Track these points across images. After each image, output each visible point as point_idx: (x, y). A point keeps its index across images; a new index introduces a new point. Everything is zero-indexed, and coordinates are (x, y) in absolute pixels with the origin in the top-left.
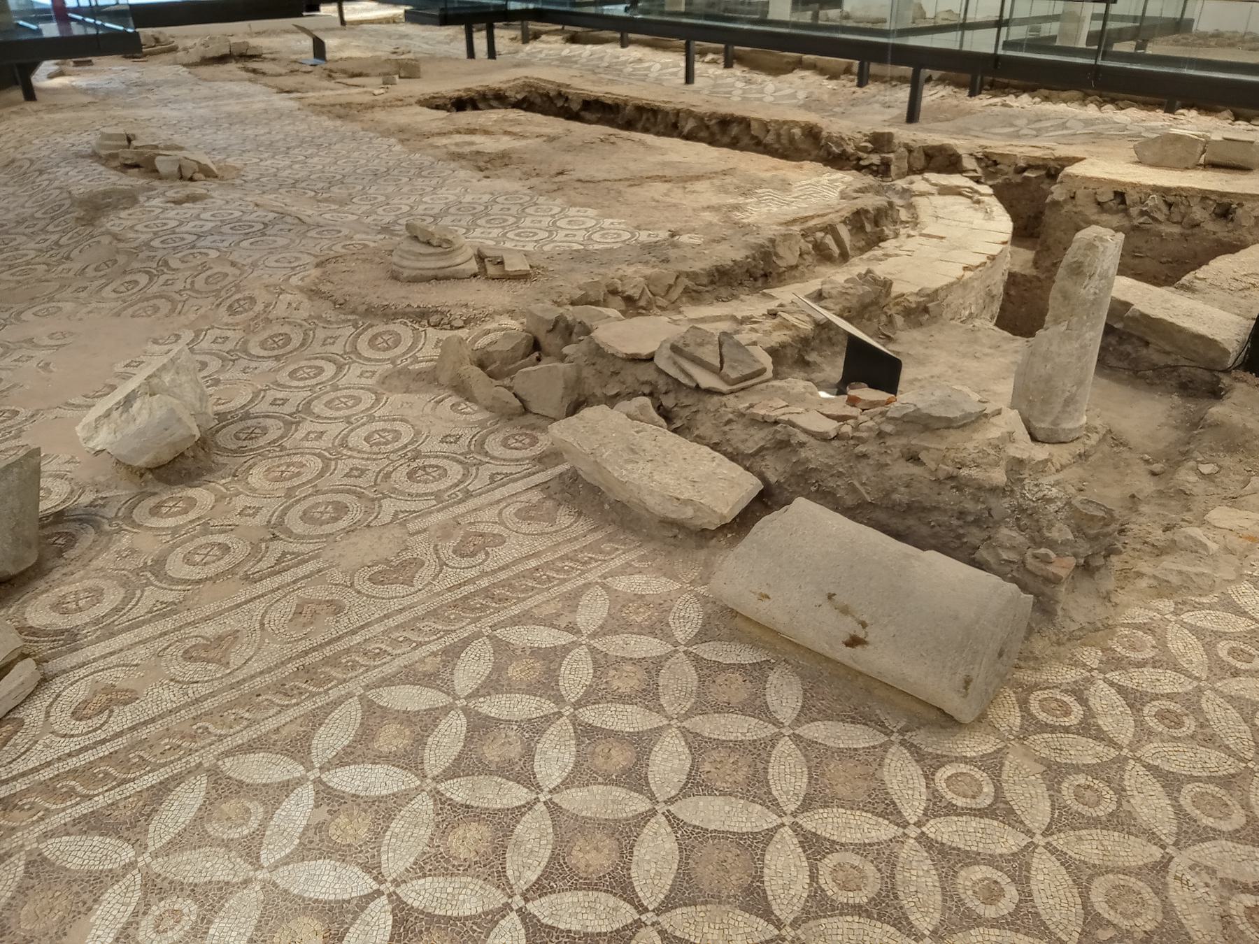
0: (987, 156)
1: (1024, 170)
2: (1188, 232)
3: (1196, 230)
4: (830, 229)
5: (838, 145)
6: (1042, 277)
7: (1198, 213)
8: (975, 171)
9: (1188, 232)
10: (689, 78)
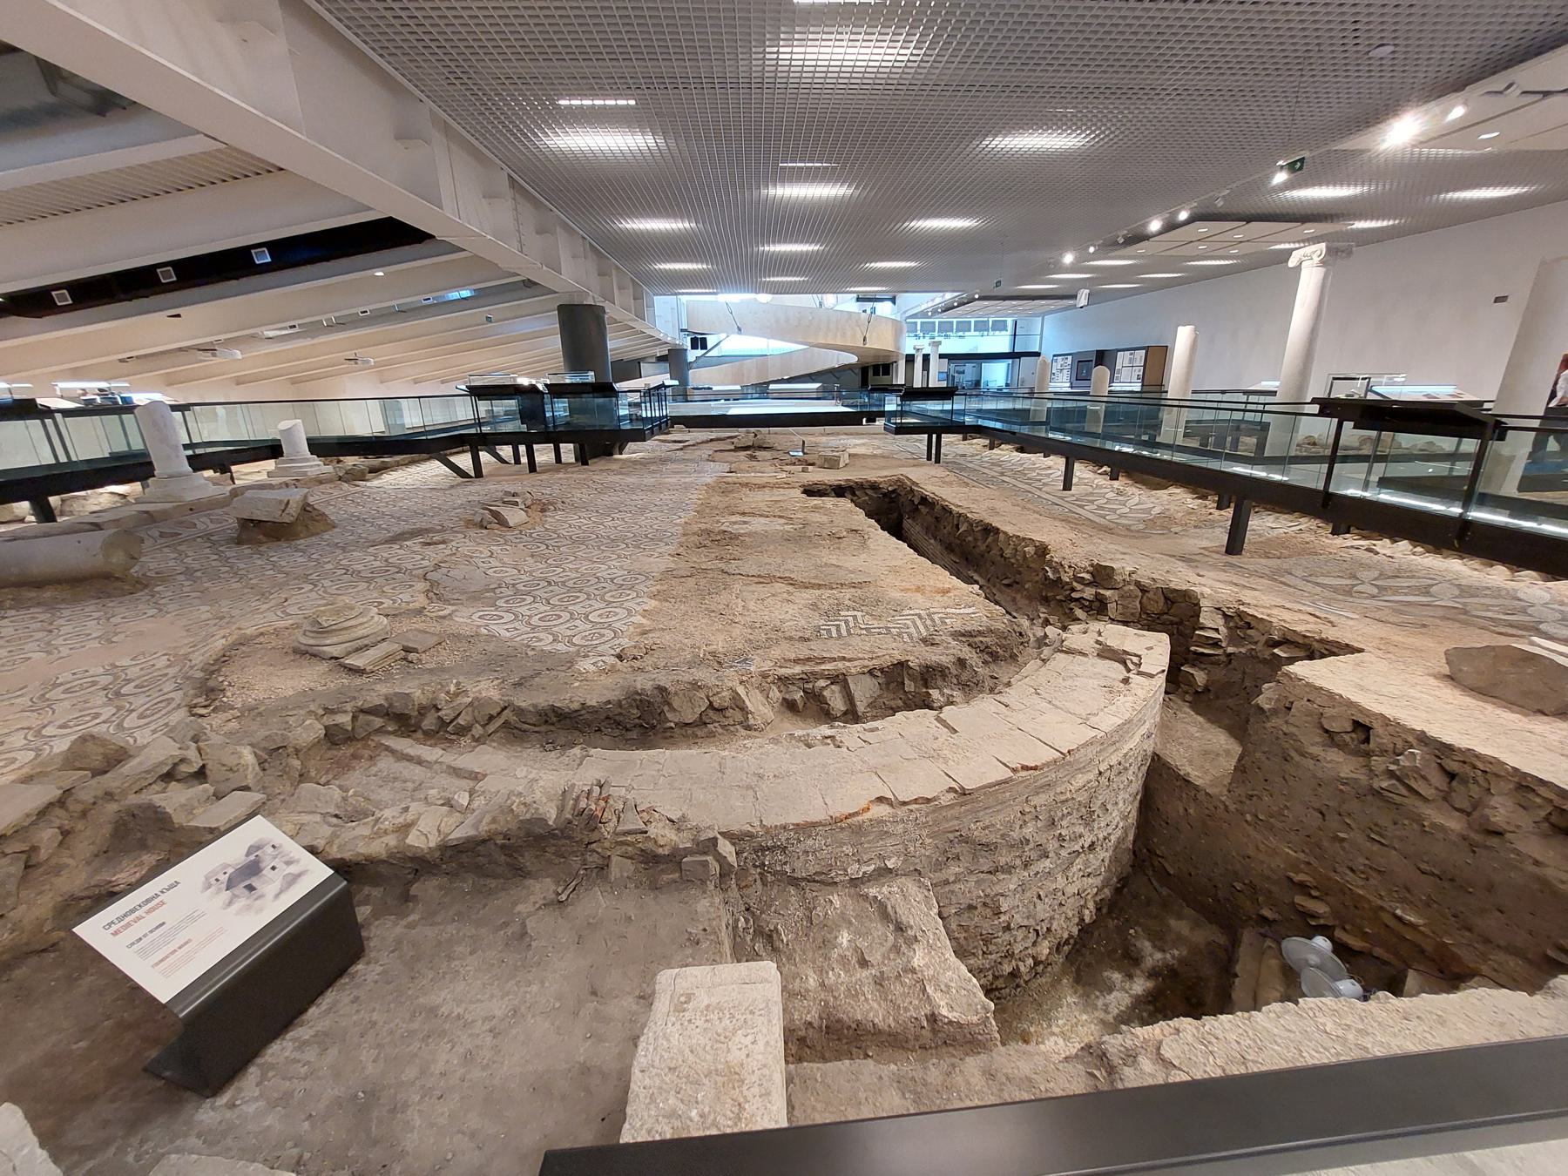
0: (1240, 614)
1: (1277, 644)
2: (1477, 837)
3: (1494, 842)
4: (839, 679)
5: (1055, 571)
6: (1232, 807)
7: (1501, 810)
8: (1217, 630)
9: (1477, 837)
10: (1067, 485)
